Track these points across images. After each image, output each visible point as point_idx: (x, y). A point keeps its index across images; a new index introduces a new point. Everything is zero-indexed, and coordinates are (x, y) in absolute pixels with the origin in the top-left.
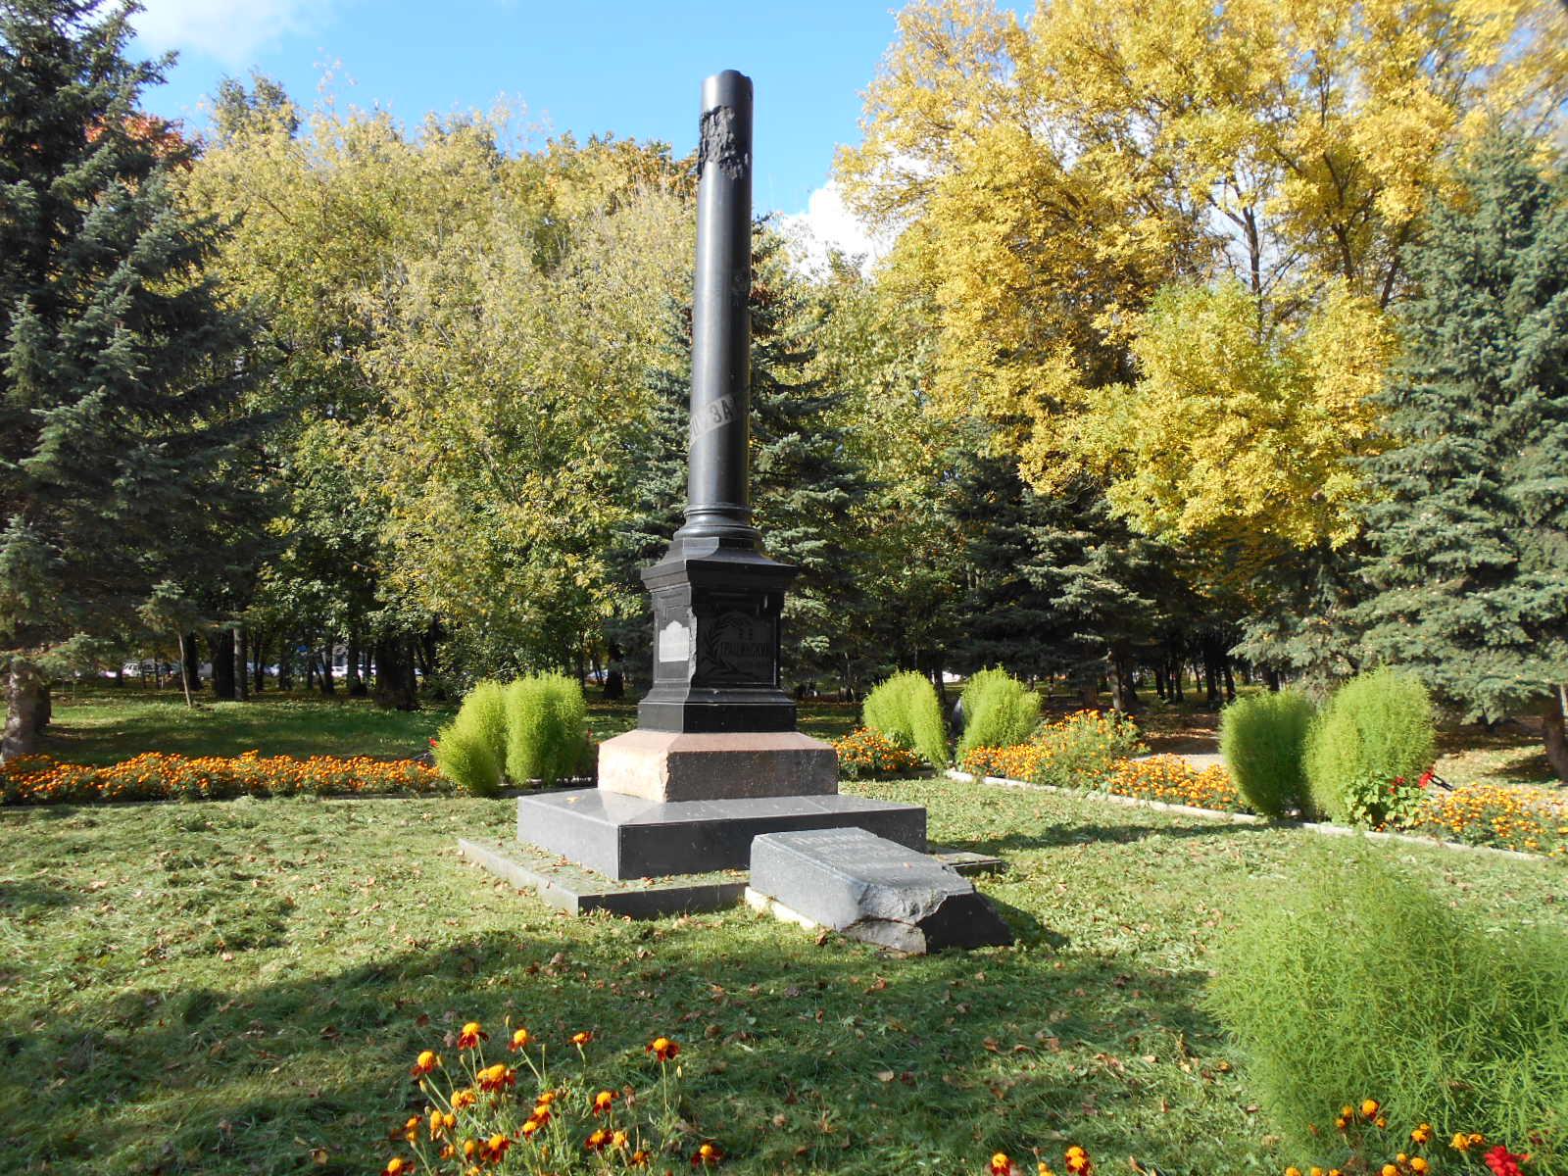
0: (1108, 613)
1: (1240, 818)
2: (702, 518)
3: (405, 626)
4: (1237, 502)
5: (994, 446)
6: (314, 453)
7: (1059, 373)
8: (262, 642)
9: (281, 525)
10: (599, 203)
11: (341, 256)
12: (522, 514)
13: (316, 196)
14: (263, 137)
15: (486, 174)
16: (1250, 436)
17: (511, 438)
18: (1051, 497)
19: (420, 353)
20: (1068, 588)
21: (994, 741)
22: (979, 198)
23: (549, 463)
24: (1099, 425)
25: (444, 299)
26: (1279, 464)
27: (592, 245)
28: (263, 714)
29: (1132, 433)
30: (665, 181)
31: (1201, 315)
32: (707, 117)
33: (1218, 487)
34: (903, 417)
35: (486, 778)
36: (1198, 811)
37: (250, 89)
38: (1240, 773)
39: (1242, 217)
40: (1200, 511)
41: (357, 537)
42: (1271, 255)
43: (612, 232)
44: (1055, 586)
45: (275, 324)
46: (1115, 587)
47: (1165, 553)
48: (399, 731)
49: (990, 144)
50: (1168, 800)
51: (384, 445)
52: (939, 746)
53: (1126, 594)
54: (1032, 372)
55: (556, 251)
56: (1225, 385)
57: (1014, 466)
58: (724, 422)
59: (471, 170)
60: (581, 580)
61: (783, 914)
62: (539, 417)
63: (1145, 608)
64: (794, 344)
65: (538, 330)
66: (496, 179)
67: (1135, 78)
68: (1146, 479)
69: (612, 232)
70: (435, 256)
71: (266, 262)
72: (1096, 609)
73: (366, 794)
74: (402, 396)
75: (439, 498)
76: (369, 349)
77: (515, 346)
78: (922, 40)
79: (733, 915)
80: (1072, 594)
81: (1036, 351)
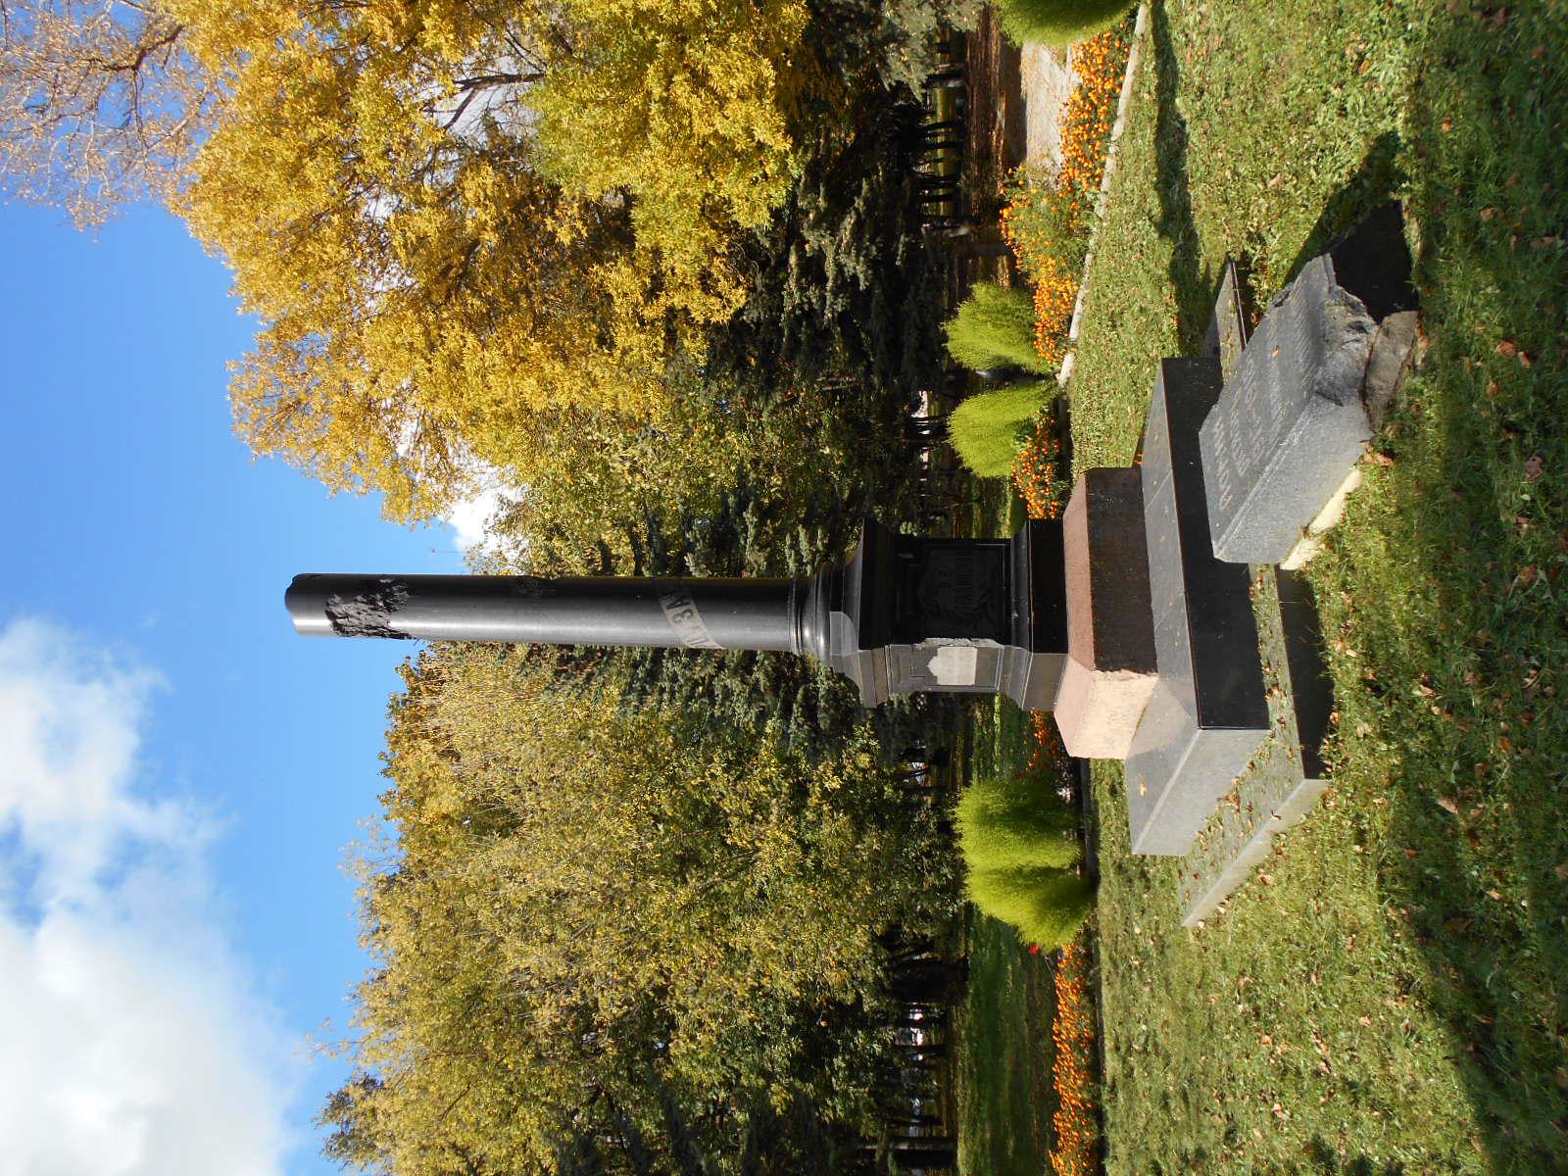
0: (876, 228)
1: (1143, 22)
2: (807, 633)
3: (880, 973)
4: (759, 89)
5: (695, 347)
6: (705, 1063)
7: (620, 279)
8: (894, 1117)
9: (778, 1098)
10: (448, 769)
11: (501, 1038)
12: (767, 848)
13: (440, 1063)
14: (380, 1117)
15: (418, 885)
16: (693, 73)
17: (685, 862)
18: (752, 290)
19: (600, 957)
20: (849, 270)
21: (1028, 333)
22: (440, 368)
23: (714, 819)
24: (677, 240)
25: (545, 931)
26: (722, 43)
27: (489, 775)
28: (973, 1122)
29: (683, 198)
30: (426, 701)
31: (565, 126)
32: (338, 627)
33: (743, 106)
34: (665, 450)
35: (1074, 893)
36: (1128, 80)
37: (333, 1128)
38: (1090, 22)
39: (467, 94)
40: (768, 129)
41: (789, 1020)
42: (505, 65)
43: (477, 755)
44: (846, 284)
45: (571, 1106)
46: (849, 222)
47: (813, 170)
48: (995, 981)
49: (387, 359)
50: (1112, 117)
51: (695, 993)
52: (1032, 392)
53: (856, 210)
54: (620, 307)
55: (495, 814)
56: (636, 100)
57: (718, 328)
58: (692, 607)
59: (415, 900)
60: (834, 784)
61: (1329, 515)
62: (667, 831)
63: (871, 189)
64: (590, 562)
65: (579, 832)
66: (424, 874)
67: (320, 199)
68: (731, 185)
69: (477, 755)
70: (502, 940)
71: (507, 1117)
72: (872, 241)
73: (1097, 1026)
74: (645, 973)
75: (754, 935)
76: (596, 1009)
77: (594, 856)
78: (282, 429)
79: (1326, 583)
80: (856, 267)
81: (598, 305)
